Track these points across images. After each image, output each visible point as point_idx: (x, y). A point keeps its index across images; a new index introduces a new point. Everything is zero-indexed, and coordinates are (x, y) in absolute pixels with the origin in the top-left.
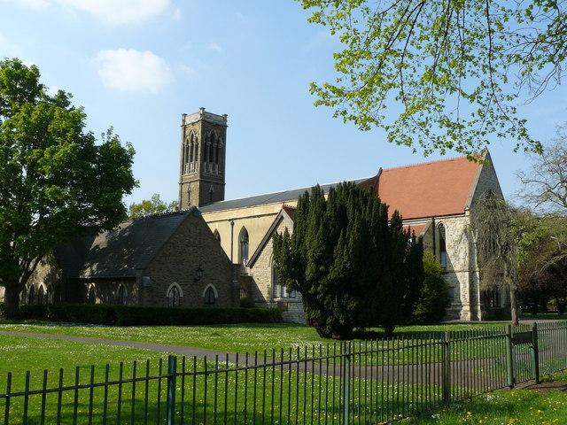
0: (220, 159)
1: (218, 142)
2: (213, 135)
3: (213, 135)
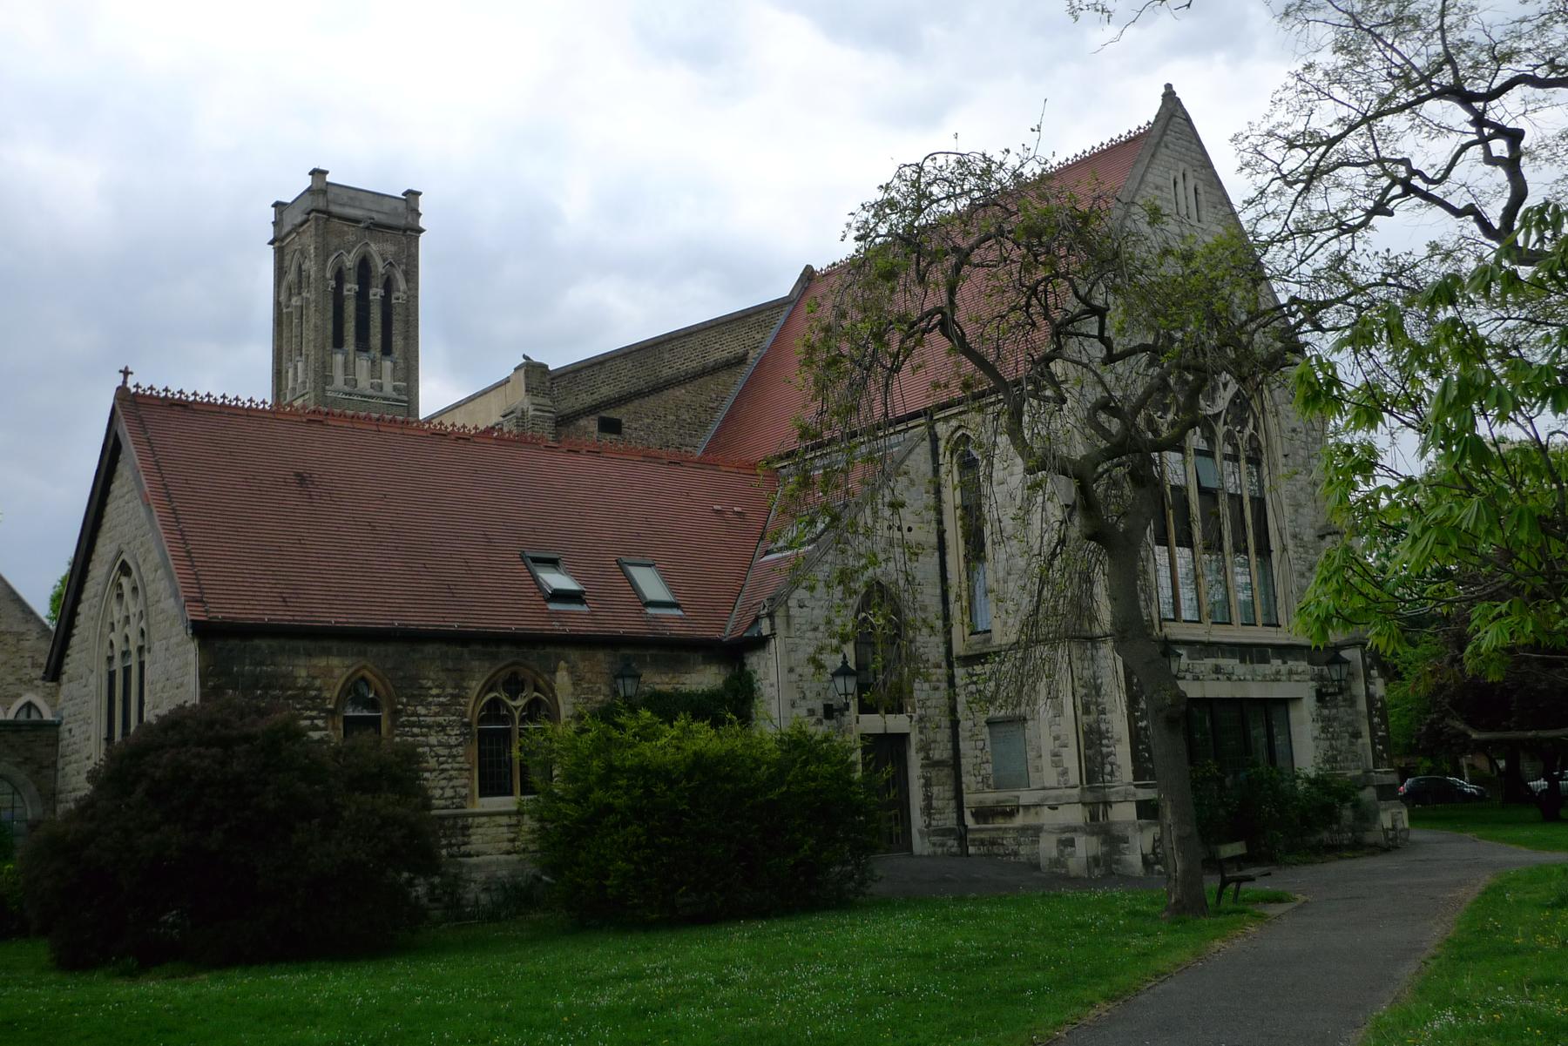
0: (398, 342)
1: (388, 285)
2: (364, 265)
3: (364, 265)
